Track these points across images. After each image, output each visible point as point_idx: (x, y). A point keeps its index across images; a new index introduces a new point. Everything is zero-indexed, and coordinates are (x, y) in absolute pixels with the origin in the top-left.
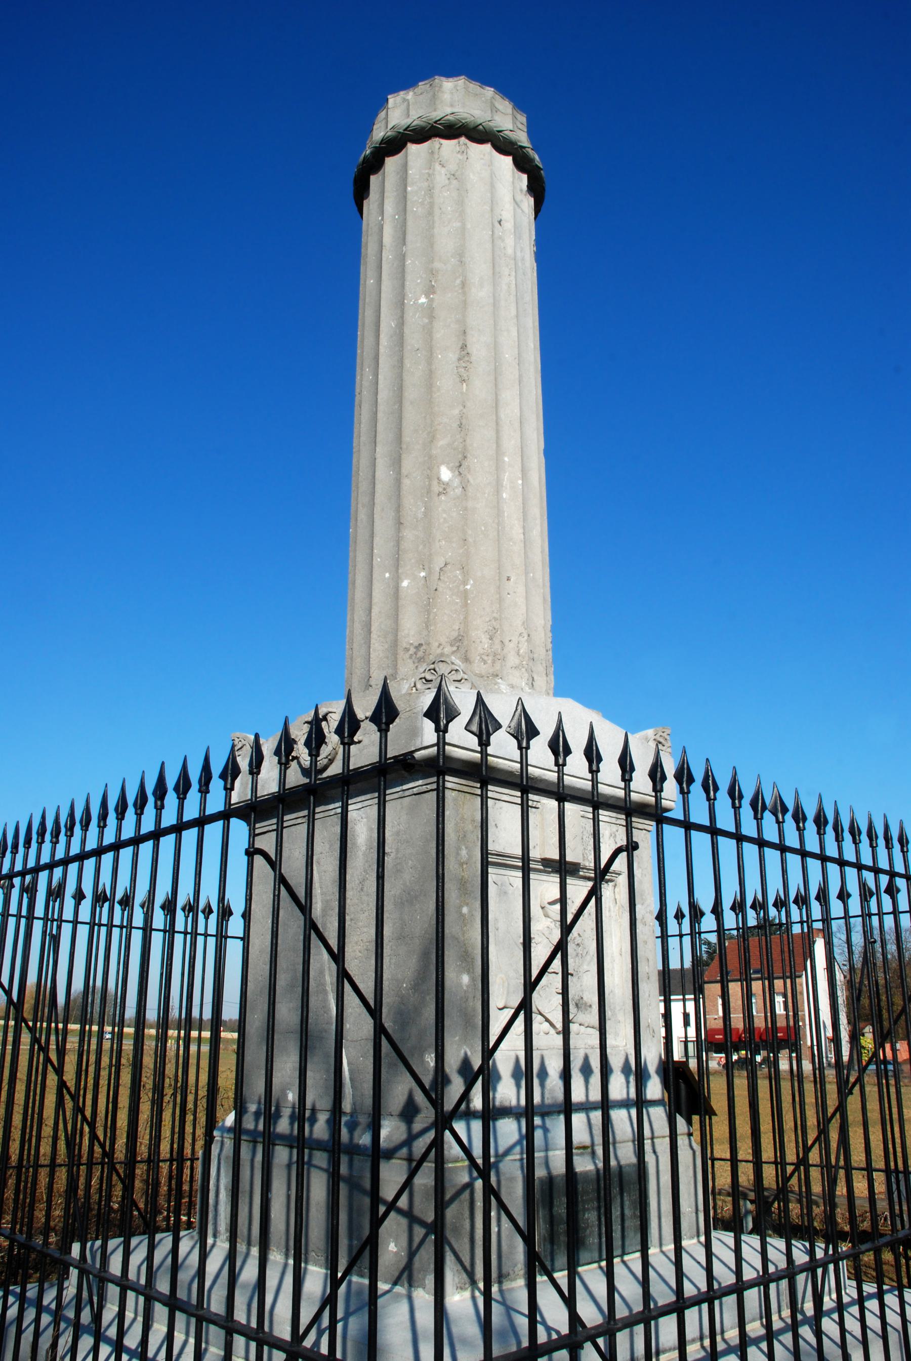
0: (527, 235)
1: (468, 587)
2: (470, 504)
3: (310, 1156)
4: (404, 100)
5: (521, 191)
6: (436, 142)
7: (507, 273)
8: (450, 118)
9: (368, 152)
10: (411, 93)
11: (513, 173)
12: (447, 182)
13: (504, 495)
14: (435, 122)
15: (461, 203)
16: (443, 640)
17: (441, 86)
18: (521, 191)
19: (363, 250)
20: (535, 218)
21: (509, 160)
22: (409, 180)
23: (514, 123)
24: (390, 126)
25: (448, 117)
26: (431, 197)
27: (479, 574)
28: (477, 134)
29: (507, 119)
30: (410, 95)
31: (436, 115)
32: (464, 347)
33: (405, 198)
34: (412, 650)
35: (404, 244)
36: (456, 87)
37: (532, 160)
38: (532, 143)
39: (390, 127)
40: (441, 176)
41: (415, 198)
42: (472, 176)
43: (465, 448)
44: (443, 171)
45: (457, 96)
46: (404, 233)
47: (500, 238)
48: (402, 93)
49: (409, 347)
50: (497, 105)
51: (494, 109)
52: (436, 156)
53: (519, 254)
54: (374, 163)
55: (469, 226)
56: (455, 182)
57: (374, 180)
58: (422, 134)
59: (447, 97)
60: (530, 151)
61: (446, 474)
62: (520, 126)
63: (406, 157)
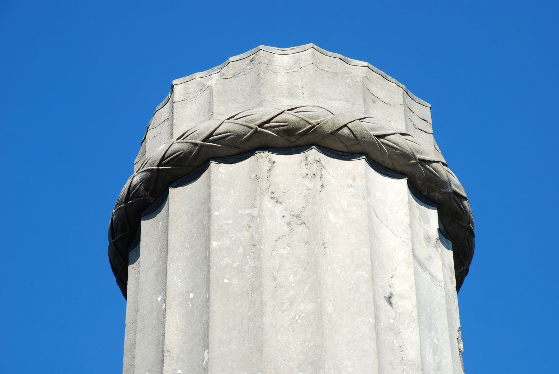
0: (445, 321)
4: (204, 88)
5: (428, 238)
6: (263, 159)
8: (289, 117)
9: (137, 179)
10: (215, 76)
11: (410, 208)
12: (286, 229)
14: (261, 125)
17: (270, 63)
18: (428, 238)
19: (126, 359)
20: (458, 288)
21: (402, 183)
22: (215, 227)
23: (408, 120)
24: (177, 133)
26: (257, 257)
28: (340, 144)
29: (394, 112)
30: (213, 78)
31: (262, 113)
33: (207, 261)
35: (206, 346)
36: (297, 62)
37: (444, 184)
38: (443, 153)
39: (177, 135)
40: (274, 218)
41: (227, 260)
42: (332, 217)
44: (279, 209)
45: (298, 80)
46: (206, 325)
47: (391, 328)
48: (198, 75)
49: (419, 182)
50: (374, 90)
51: (369, 97)
52: (265, 185)
53: (429, 358)
54: (149, 197)
55: (330, 309)
56: (300, 229)
57: (147, 227)
58: (235, 148)
59: (282, 80)
60: (439, 166)
62: (420, 124)
63: (209, 186)
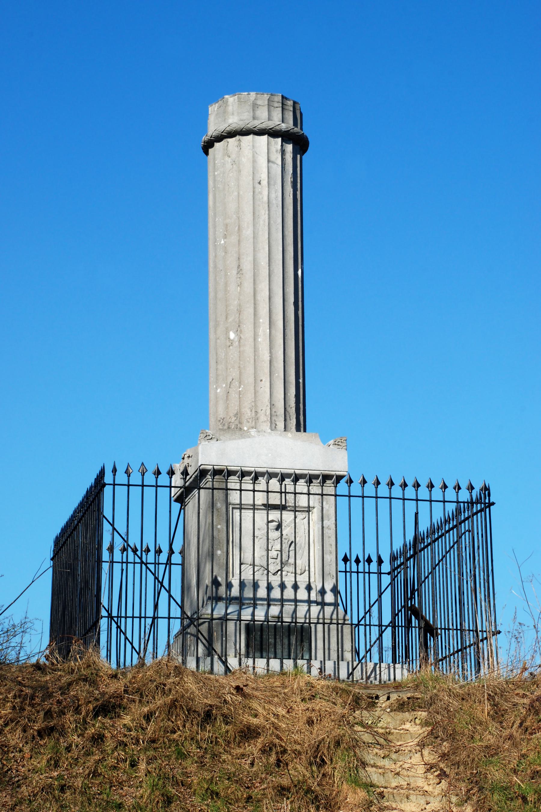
1: (241, 389)
2: (242, 349)
3: (262, 605)
7: (263, 213)
8: (228, 129)
12: (231, 166)
13: (259, 340)
15: (238, 180)
16: (232, 415)
25: (227, 129)
27: (246, 382)
32: (239, 266)
34: (222, 421)
43: (240, 322)
54: (208, 146)
61: (232, 335)
